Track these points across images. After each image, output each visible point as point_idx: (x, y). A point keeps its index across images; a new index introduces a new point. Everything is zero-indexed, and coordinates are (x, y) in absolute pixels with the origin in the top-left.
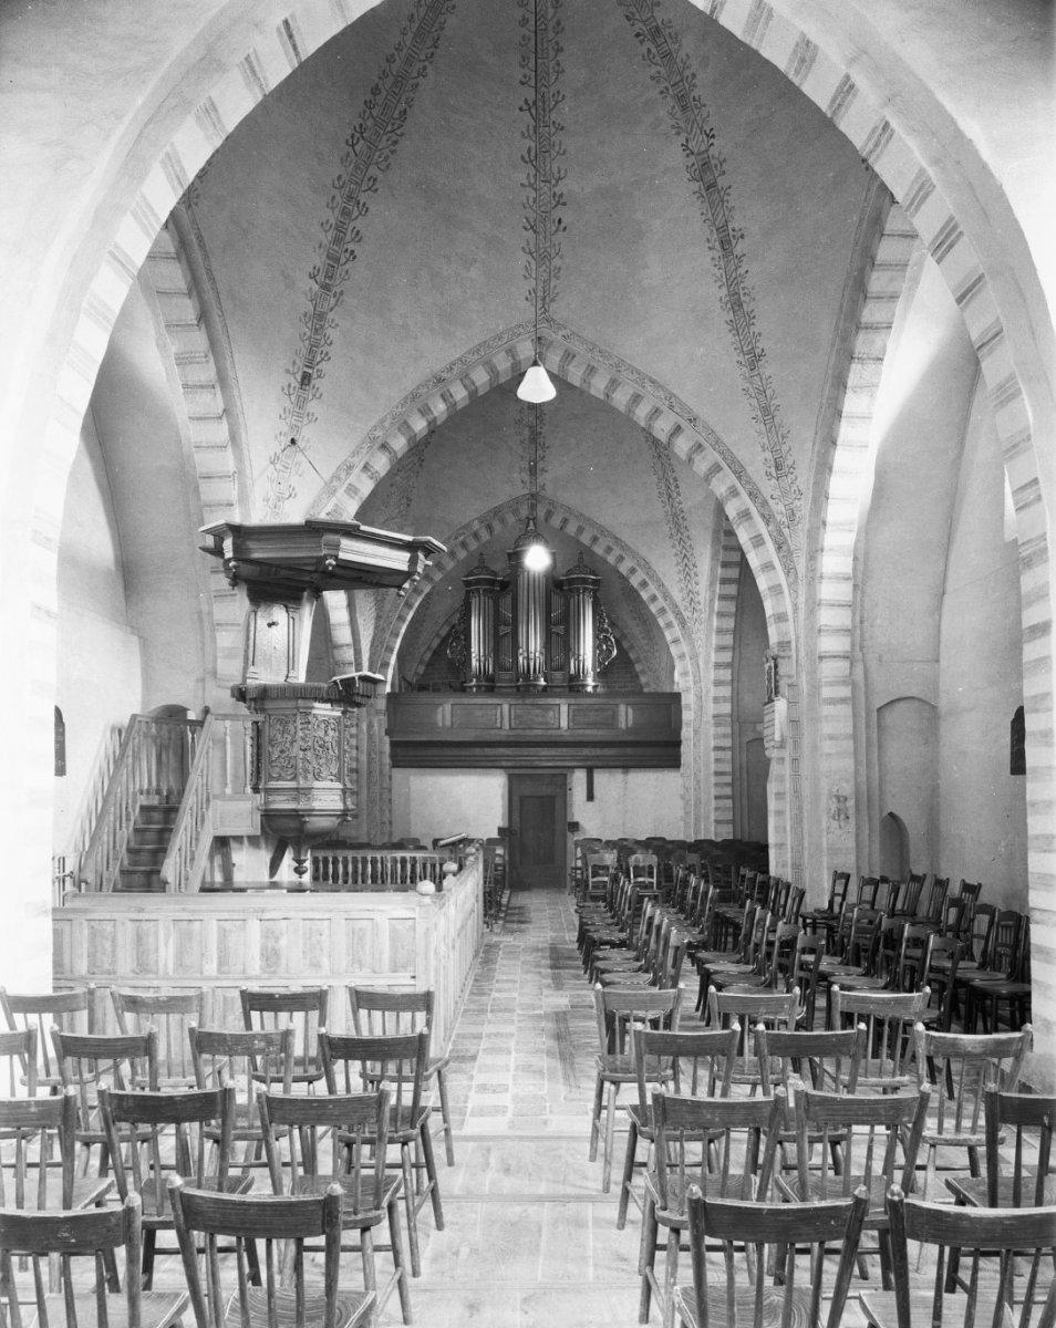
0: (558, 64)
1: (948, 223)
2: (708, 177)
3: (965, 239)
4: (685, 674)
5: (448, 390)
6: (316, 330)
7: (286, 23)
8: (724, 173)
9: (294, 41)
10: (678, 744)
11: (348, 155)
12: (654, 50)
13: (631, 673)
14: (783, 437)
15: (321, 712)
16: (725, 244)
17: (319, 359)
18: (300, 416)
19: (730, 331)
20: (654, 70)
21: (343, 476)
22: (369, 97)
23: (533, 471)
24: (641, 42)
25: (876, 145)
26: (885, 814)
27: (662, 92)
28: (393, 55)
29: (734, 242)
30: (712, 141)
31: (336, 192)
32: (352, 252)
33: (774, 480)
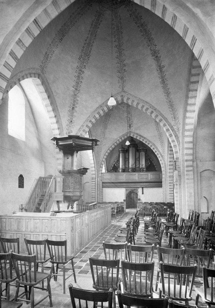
0: (122, 36)
2: (156, 55)
3: (197, 40)
5: (103, 108)
9: (38, 24)
10: (161, 182)
11: (79, 61)
12: (142, 29)
13: (154, 168)
18: (72, 116)
20: (142, 33)
23: (130, 126)
24: (139, 28)
27: (144, 38)
29: (162, 68)
31: (77, 69)
32: (81, 81)
33: (174, 121)
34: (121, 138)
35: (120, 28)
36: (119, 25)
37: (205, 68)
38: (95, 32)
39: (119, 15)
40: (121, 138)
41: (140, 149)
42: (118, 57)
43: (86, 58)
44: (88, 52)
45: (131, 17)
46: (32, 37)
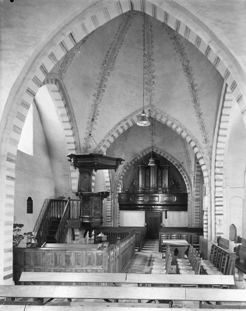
0: (152, 45)
1: (234, 82)
4: (189, 189)
6: (95, 108)
7: (71, 34)
8: (192, 70)
10: (187, 205)
11: (102, 67)
14: (207, 133)
15: (95, 199)
16: (192, 87)
17: (96, 115)
19: (194, 108)
21: (102, 143)
22: (107, 53)
24: (172, 40)
25: (217, 63)
26: (231, 224)
27: (177, 52)
28: (112, 44)
29: (195, 87)
30: (189, 63)
32: (104, 90)
34: (143, 154)
35: (150, 36)
36: (150, 33)
37: (243, 112)
38: (123, 36)
39: (151, 22)
40: (143, 154)
41: (163, 167)
42: (147, 67)
43: (111, 64)
44: (114, 58)
45: (163, 26)
46: (65, 50)
